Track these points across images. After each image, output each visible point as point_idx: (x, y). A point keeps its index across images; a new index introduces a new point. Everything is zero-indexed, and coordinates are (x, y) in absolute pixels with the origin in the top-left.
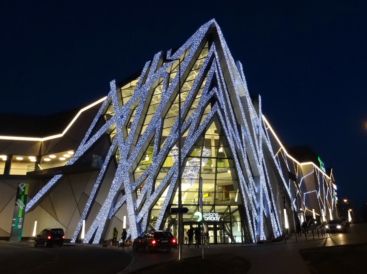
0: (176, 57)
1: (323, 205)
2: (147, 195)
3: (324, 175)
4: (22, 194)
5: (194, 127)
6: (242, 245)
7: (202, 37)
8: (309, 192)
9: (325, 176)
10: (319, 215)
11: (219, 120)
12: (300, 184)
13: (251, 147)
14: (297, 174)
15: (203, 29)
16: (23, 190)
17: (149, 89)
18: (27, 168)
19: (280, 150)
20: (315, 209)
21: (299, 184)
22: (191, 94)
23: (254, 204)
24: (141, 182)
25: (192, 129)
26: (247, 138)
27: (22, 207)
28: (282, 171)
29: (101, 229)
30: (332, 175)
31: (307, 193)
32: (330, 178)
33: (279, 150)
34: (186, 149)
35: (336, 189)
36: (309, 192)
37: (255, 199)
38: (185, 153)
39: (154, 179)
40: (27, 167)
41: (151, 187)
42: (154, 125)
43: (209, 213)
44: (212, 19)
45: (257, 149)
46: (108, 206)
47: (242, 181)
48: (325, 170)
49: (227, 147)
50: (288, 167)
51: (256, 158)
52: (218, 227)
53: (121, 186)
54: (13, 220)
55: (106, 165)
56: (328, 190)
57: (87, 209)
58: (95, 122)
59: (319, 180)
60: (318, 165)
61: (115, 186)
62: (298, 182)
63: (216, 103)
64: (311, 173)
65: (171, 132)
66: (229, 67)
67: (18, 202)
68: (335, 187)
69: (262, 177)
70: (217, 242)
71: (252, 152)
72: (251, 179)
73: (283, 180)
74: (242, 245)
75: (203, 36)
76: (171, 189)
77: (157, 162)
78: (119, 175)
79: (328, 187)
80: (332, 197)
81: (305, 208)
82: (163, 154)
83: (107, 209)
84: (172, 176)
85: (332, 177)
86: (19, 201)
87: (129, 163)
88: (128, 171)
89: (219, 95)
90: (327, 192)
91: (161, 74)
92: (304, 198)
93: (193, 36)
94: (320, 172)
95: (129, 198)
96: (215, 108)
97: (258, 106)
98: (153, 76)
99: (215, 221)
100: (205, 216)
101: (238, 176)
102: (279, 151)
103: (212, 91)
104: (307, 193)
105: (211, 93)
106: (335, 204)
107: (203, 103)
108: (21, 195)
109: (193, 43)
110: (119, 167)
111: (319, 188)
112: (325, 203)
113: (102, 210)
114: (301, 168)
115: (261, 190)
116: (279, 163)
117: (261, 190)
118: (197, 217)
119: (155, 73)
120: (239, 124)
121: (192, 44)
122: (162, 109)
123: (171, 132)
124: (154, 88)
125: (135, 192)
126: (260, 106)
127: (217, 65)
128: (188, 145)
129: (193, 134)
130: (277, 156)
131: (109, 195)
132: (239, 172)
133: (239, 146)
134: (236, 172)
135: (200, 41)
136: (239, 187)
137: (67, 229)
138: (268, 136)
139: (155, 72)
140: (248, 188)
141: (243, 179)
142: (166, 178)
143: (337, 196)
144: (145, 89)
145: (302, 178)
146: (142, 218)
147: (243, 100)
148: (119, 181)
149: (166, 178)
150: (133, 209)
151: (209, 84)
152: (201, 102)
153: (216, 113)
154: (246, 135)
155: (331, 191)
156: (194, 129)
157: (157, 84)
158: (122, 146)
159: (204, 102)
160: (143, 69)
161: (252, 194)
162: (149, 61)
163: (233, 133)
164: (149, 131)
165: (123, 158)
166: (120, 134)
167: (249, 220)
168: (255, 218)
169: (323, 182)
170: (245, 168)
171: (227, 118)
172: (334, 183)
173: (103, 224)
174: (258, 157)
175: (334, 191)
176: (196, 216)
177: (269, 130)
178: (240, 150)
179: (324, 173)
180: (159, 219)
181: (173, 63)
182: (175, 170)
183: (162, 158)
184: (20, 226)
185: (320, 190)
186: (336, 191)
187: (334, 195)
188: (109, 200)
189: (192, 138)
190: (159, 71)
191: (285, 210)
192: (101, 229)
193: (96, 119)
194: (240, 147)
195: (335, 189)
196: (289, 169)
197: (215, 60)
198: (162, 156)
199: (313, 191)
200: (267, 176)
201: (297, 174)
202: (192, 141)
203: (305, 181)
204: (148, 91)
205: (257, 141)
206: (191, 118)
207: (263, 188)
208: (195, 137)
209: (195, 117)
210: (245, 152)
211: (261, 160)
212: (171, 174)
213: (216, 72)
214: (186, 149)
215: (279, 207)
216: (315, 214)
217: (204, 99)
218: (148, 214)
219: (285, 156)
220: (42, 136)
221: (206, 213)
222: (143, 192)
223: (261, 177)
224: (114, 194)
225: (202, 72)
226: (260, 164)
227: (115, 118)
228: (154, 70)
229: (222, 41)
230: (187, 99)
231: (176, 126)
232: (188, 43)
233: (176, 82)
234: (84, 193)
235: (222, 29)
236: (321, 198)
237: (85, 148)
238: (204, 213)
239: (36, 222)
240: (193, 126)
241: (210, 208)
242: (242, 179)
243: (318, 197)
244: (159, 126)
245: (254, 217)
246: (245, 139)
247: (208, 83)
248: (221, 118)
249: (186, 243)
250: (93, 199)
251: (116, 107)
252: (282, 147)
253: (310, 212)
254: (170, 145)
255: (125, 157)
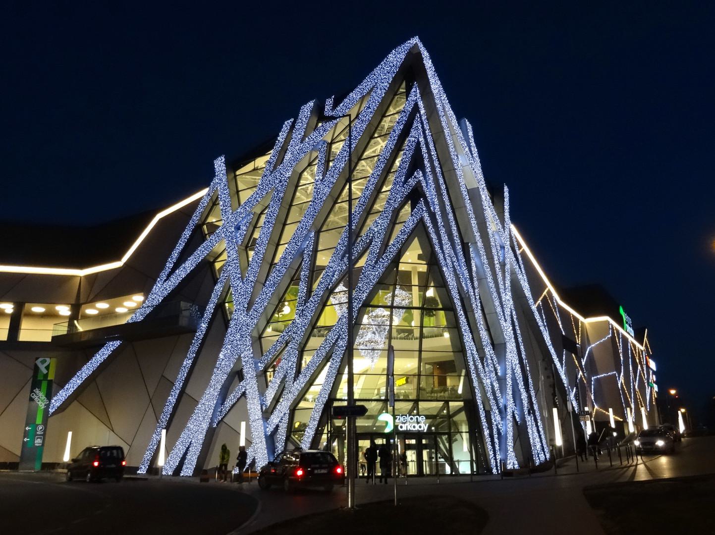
0: (342, 112)
1: (630, 400)
2: (286, 381)
3: (632, 342)
4: (42, 379)
5: (378, 248)
6: (472, 478)
7: (394, 72)
8: (602, 376)
9: (633, 343)
10: (622, 420)
11: (428, 234)
12: (585, 360)
13: (488, 286)
14: (579, 340)
15: (396, 57)
16: (45, 371)
17: (290, 173)
18: (54, 328)
19: (545, 293)
20: (613, 409)
21: (583, 359)
22: (373, 184)
23: (495, 398)
24: (274, 355)
25: (374, 252)
26: (481, 270)
27: (43, 404)
28: (550, 335)
29: (196, 446)
30: (646, 341)
31: (598, 377)
32: (643, 348)
33: (544, 294)
34: (361, 290)
35: (655, 369)
36: (602, 376)
37: (496, 389)
38: (360, 299)
39: (300, 350)
40: (53, 325)
41: (295, 364)
42: (299, 244)
43: (406, 416)
44: (413, 37)
45: (502, 290)
46: (210, 403)
47: (471, 353)
48: (633, 331)
49: (441, 287)
50: (561, 326)
51: (499, 309)
52: (424, 444)
53: (236, 363)
54: (25, 430)
55: (206, 323)
56: (640, 371)
57: (169, 409)
58: (185, 238)
59: (621, 351)
60: (620, 322)
61: (223, 363)
62: (580, 355)
63: (421, 201)
64: (606, 338)
65: (332, 257)
66: (446, 131)
67: (36, 394)
68: (653, 365)
69: (511, 346)
70: (423, 472)
71: (492, 297)
72: (488, 350)
73: (552, 351)
74: (472, 478)
75: (395, 71)
76: (334, 370)
77: (306, 316)
78: (232, 342)
79: (639, 366)
80: (646, 384)
81: (593, 407)
82: (318, 300)
83: (209, 409)
84: (334, 344)
85: (646, 346)
86: (37, 392)
87: (252, 319)
88: (249, 335)
89: (427, 185)
90: (638, 374)
91: (314, 145)
92: (593, 387)
93: (377, 71)
94: (623, 337)
95: (251, 387)
96: (419, 210)
97: (504, 208)
98: (297, 147)
99: (419, 431)
100: (399, 421)
101: (464, 343)
102: (543, 296)
103: (413, 177)
104: (598, 377)
105: (412, 182)
106: (654, 398)
107: (395, 201)
108: (40, 382)
109: (376, 83)
110: (232, 326)
111: (622, 367)
112: (632, 396)
113: (198, 410)
114: (587, 328)
115: (509, 372)
116: (544, 317)
117: (509, 372)
118: (384, 424)
119: (302, 142)
120: (465, 242)
121: (374, 87)
122: (316, 212)
123: (332, 257)
124: (300, 172)
125: (264, 375)
126: (507, 207)
127: (423, 127)
128: (366, 283)
129: (376, 263)
130: (539, 304)
131: (212, 381)
132: (465, 336)
133: (466, 285)
134: (461, 336)
135: (389, 79)
136: (466, 365)
137: (130, 446)
138: (522, 266)
139: (302, 140)
140: (484, 367)
141: (473, 350)
142: (323, 347)
143: (656, 383)
144: (282, 174)
145: (589, 348)
146: (277, 426)
147: (474, 194)
148: (232, 353)
149: (323, 347)
150: (259, 408)
151: (406, 165)
152: (391, 200)
153: (421, 221)
154: (479, 264)
155: (645, 372)
156: (379, 253)
157: (307, 165)
158: (238, 286)
159: (398, 199)
160: (278, 135)
161: (490, 378)
162: (290, 119)
163: (455, 259)
164: (289, 255)
165: (239, 309)
166: (233, 261)
167: (485, 430)
168: (497, 425)
169: (630, 355)
170: (477, 328)
171: (443, 231)
172: (651, 357)
173: (201, 437)
174: (502, 307)
175: (651, 373)
176: (382, 422)
177: (523, 254)
178: (467, 293)
179: (632, 337)
180: (309, 428)
181: (337, 124)
182: (342, 331)
183: (317, 309)
184: (38, 442)
185: (624, 371)
186: (654, 373)
187: (650, 381)
188: (212, 390)
189: (373, 269)
190: (309, 139)
191: (555, 411)
192: (196, 446)
193: (187, 233)
194: (467, 287)
195: (652, 369)
196: (562, 330)
197: (418, 118)
198: (316, 304)
199: (609, 374)
200: (520, 344)
201: (580, 339)
202: (375, 276)
203: (594, 353)
204: (289, 177)
205: (501, 275)
206: (372, 230)
207: (512, 366)
208: (379, 268)
209: (380, 229)
210: (478, 297)
211: (508, 313)
212: (333, 340)
213: (420, 140)
214: (361, 290)
215: (544, 404)
216: (615, 419)
217: (397, 194)
218: (289, 419)
219: (555, 304)
220: (81, 265)
221: (402, 416)
222: (279, 376)
223: (508, 345)
224: (222, 379)
225: (394, 140)
226: (506, 321)
227: (225, 230)
228: (299, 136)
229: (432, 81)
230: (365, 194)
231: (342, 247)
232: (366, 84)
233: (344, 160)
234: (164, 377)
235: (432, 57)
236: (624, 387)
237: (166, 289)
238: (397, 417)
239: (70, 434)
240: (376, 245)
241: (409, 405)
242: (471, 350)
243: (619, 385)
244: (310, 246)
245: (495, 423)
246: (477, 272)
247: (406, 162)
248: (431, 230)
249: (363, 474)
250: (182, 388)
251: (226, 209)
252: (550, 287)
253: (605, 413)
254: (332, 283)
255: (244, 306)
